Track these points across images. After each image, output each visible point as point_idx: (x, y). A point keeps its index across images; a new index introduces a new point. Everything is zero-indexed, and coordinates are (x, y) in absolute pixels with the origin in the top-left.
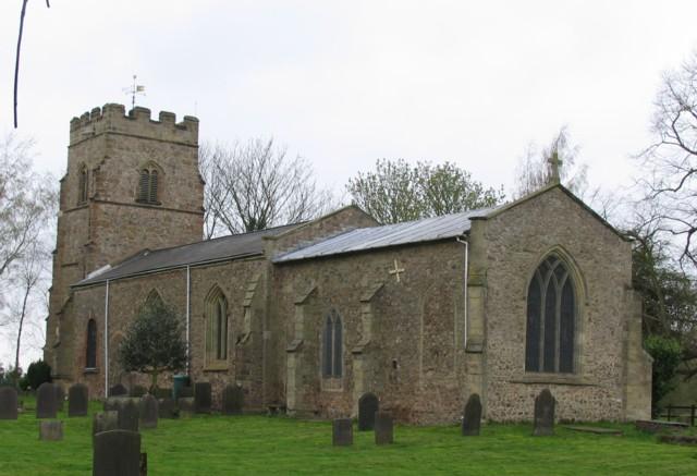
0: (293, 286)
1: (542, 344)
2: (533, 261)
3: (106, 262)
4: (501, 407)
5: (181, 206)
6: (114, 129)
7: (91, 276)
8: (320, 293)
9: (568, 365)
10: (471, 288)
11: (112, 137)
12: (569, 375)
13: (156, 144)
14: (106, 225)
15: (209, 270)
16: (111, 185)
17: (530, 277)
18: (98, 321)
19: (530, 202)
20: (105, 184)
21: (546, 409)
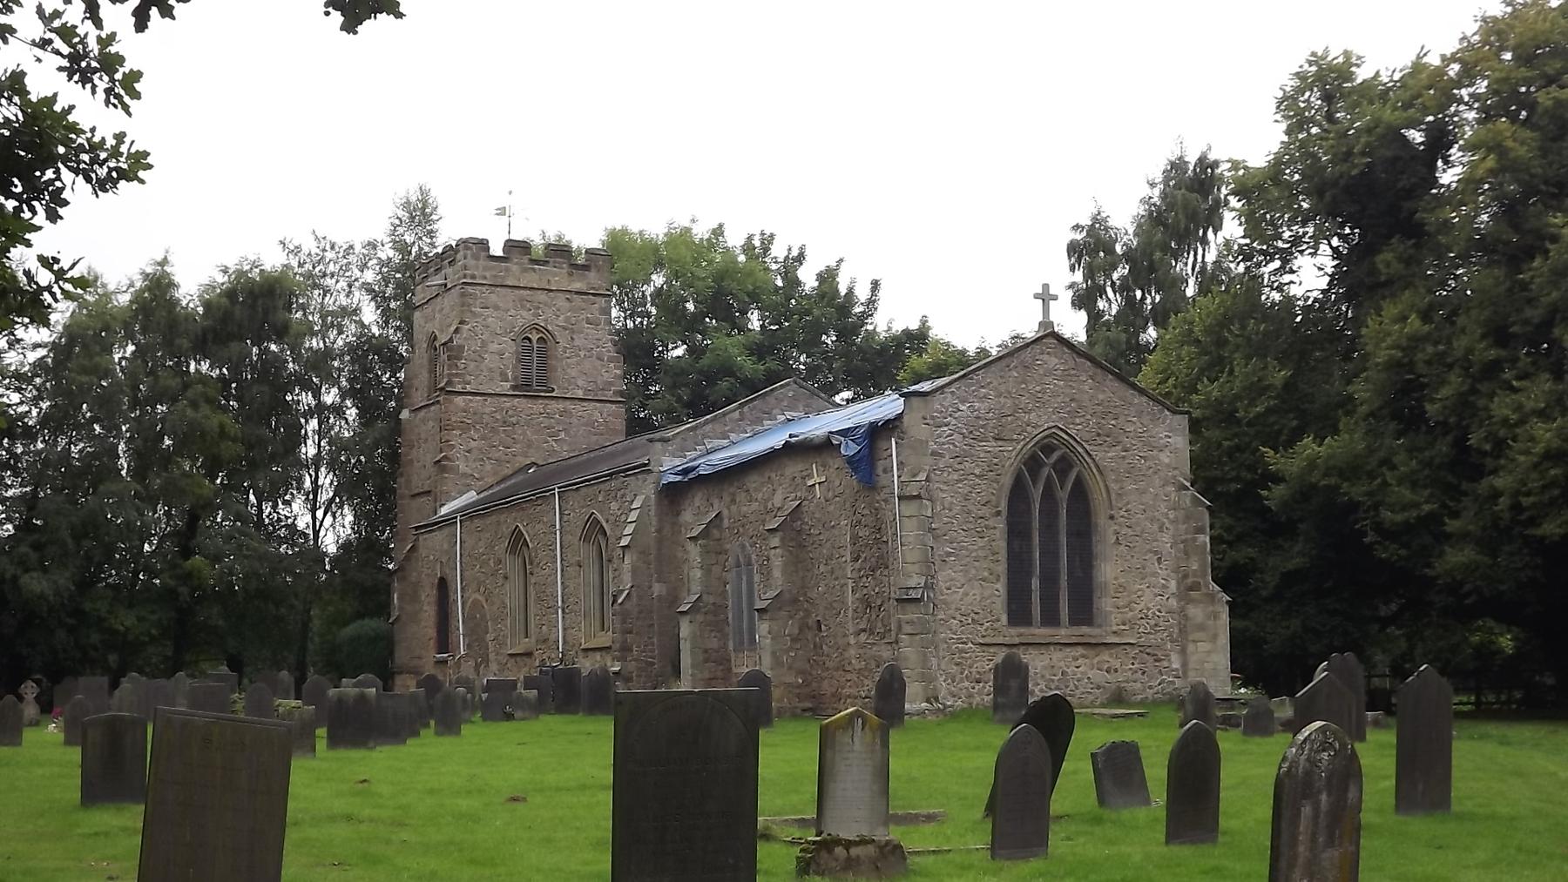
0: (695, 516)
1: (1035, 583)
2: (1012, 455)
3: (468, 488)
4: (966, 684)
5: (587, 391)
6: (473, 277)
7: (444, 511)
8: (726, 523)
9: (1084, 612)
10: (904, 503)
11: (470, 289)
12: (1085, 629)
13: (542, 296)
14: (465, 428)
15: (583, 491)
16: (472, 365)
17: (1007, 481)
18: (449, 578)
19: (1003, 363)
20: (461, 363)
21: (1014, 684)
